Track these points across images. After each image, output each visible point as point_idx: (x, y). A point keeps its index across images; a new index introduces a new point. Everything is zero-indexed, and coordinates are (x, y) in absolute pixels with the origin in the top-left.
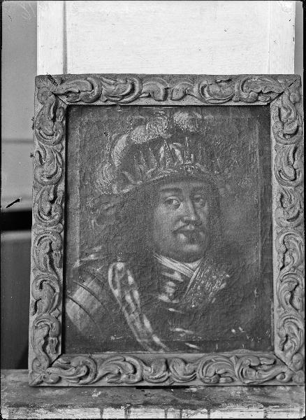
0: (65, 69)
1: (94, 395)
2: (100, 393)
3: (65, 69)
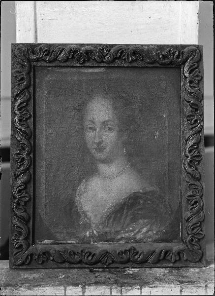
0: (36, 38)
1: (60, 277)
3: (36, 38)
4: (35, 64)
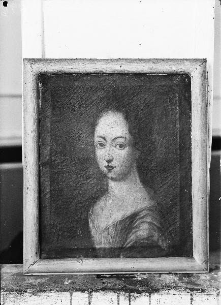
2: (70, 281)
4: (64, 95)
